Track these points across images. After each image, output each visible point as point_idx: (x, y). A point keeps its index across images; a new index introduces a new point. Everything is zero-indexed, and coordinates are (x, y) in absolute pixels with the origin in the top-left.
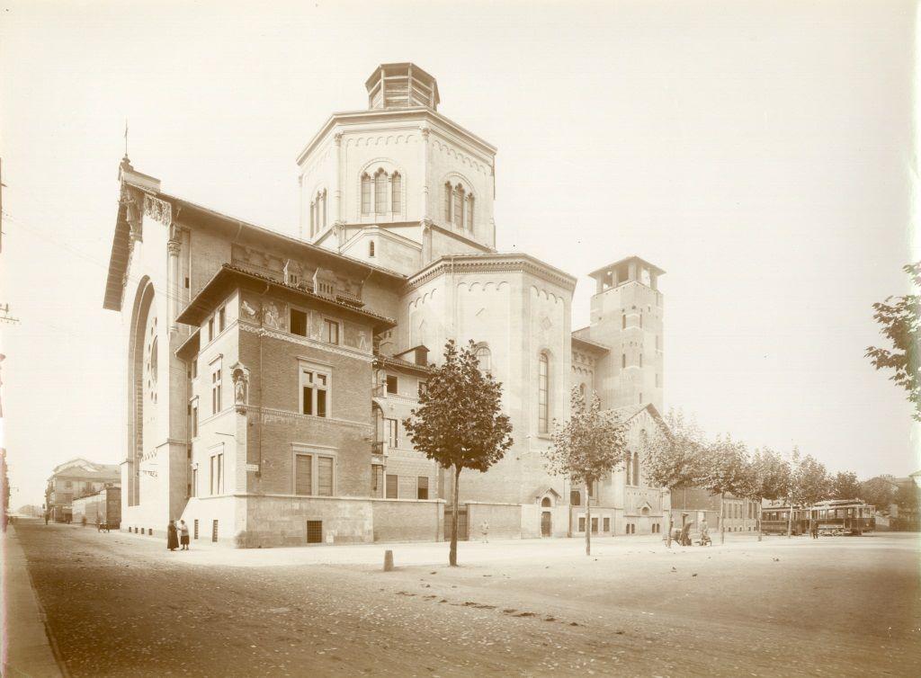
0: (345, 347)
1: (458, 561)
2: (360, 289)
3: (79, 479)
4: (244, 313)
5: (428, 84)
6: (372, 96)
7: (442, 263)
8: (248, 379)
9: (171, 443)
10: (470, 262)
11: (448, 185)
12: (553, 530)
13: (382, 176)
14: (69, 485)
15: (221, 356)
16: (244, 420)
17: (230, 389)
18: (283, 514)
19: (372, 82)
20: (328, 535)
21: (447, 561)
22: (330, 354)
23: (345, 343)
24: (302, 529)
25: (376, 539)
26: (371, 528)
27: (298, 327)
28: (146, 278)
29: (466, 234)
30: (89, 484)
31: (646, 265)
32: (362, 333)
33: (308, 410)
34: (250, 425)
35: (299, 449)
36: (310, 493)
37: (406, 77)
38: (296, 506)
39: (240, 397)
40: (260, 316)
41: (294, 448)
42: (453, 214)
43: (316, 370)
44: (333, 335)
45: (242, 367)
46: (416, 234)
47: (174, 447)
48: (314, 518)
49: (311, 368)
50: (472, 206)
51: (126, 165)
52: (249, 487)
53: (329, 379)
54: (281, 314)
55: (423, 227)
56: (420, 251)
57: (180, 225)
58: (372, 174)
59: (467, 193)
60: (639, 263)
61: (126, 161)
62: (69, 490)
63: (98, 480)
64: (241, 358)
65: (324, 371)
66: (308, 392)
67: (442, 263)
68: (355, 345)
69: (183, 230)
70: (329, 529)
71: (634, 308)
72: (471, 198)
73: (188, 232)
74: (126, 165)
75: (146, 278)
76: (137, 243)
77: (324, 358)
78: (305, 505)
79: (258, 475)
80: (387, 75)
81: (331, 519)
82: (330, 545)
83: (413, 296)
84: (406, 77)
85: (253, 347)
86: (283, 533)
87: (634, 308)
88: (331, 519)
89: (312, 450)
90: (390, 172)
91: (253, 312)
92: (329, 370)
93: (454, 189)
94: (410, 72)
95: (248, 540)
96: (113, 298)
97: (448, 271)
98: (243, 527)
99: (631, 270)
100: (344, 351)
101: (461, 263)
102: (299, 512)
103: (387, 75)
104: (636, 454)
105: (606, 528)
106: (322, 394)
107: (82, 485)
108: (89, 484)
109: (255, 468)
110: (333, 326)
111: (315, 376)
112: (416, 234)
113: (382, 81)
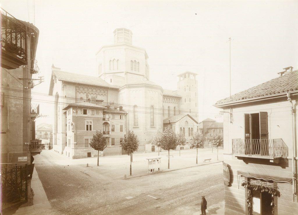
0: (96, 115)
1: (99, 165)
2: (108, 92)
3: (43, 131)
4: (73, 112)
5: (129, 32)
6: (115, 35)
7: (126, 86)
8: (74, 125)
9: (62, 133)
10: (132, 86)
11: (132, 61)
12: (155, 150)
13: (115, 60)
14: (41, 133)
15: (70, 119)
16: (74, 133)
17: (71, 127)
18: (82, 152)
19: (115, 32)
20: (92, 156)
21: (97, 165)
22: (92, 117)
23: (96, 114)
24: (86, 154)
25: (104, 155)
26: (103, 153)
27: (85, 113)
28: (57, 93)
29: (137, 73)
30: (46, 132)
31: (192, 74)
32: (100, 111)
33: (87, 129)
34: (75, 134)
35: (85, 138)
36: (88, 147)
37: (122, 31)
38: (85, 150)
39: (73, 129)
40: (77, 112)
41: (84, 138)
42: (133, 68)
43: (89, 121)
44: (93, 113)
45: (73, 123)
46: (123, 75)
47: (63, 134)
48: (89, 152)
49: (88, 121)
50: (139, 65)
51: (53, 67)
52: (75, 146)
53: (92, 122)
54: (81, 111)
55: (125, 73)
56: (124, 79)
57: (64, 84)
58: (112, 60)
59: (137, 62)
60: (189, 73)
61: (53, 65)
62: (41, 134)
63: (48, 131)
64: (73, 122)
65: (90, 121)
66: (87, 126)
67: (126, 86)
68: (99, 114)
69: (64, 85)
70: (93, 154)
71: (187, 86)
72: (138, 63)
73: (66, 85)
74: (53, 67)
75: (57, 93)
76: (56, 83)
77: (91, 118)
78: (87, 149)
79: (77, 144)
80: (118, 31)
81: (93, 152)
82: (93, 157)
83: (120, 93)
84: (122, 31)
85: (75, 119)
86: (82, 156)
87: (187, 86)
88: (93, 152)
89: (88, 138)
90: (117, 59)
91: (75, 112)
92: (92, 120)
93: (133, 62)
94: (123, 30)
95: (75, 158)
96: (51, 94)
97: (127, 88)
98: (73, 155)
99: (187, 75)
100: (96, 116)
101: (130, 86)
102: (85, 151)
103: (118, 31)
104: (184, 128)
105: (183, 149)
106: (91, 126)
107: (44, 133)
108: (46, 132)
109: (76, 143)
110: (93, 111)
111: (89, 122)
112: (123, 75)
113: (116, 32)
